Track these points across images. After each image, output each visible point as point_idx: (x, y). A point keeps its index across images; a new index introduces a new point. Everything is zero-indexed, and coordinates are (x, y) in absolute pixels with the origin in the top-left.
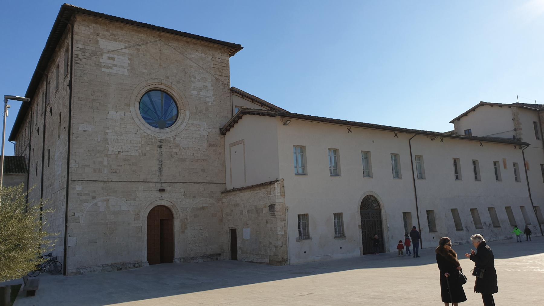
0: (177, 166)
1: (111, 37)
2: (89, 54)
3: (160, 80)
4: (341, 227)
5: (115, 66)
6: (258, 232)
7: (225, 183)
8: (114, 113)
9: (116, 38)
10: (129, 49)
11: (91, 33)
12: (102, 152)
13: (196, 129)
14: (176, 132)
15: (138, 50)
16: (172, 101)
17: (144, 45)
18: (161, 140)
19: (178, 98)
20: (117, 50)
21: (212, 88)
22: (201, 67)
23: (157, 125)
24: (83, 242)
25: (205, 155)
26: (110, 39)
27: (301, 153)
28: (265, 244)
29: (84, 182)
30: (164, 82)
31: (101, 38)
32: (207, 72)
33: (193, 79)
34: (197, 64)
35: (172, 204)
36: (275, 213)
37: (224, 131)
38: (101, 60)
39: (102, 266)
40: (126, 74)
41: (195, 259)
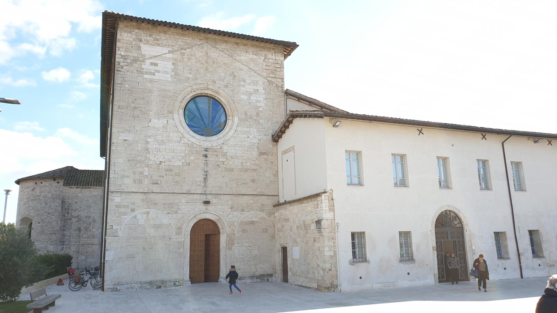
0: (224, 176)
1: (154, 42)
2: (131, 60)
3: (206, 85)
4: (409, 249)
5: (158, 72)
6: (306, 252)
7: (278, 196)
8: (157, 121)
9: (159, 42)
10: (173, 54)
11: (133, 39)
12: (143, 162)
13: (245, 136)
14: (223, 139)
15: (183, 54)
16: (220, 106)
17: (189, 48)
18: (207, 148)
19: (226, 103)
20: (161, 55)
21: (264, 92)
22: (252, 69)
23: (204, 133)
24: (120, 257)
25: (255, 164)
26: (153, 44)
27: (401, 162)
28: (313, 266)
29: (122, 194)
30: (211, 87)
31: (144, 44)
32: (259, 74)
33: (242, 83)
34: (248, 67)
35: (218, 218)
36: (322, 230)
37: (277, 138)
38: (143, 66)
39: (140, 283)
40: (170, 79)
41: (243, 279)
